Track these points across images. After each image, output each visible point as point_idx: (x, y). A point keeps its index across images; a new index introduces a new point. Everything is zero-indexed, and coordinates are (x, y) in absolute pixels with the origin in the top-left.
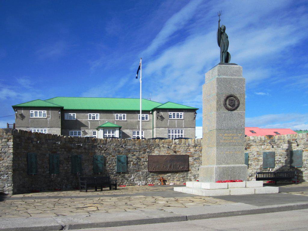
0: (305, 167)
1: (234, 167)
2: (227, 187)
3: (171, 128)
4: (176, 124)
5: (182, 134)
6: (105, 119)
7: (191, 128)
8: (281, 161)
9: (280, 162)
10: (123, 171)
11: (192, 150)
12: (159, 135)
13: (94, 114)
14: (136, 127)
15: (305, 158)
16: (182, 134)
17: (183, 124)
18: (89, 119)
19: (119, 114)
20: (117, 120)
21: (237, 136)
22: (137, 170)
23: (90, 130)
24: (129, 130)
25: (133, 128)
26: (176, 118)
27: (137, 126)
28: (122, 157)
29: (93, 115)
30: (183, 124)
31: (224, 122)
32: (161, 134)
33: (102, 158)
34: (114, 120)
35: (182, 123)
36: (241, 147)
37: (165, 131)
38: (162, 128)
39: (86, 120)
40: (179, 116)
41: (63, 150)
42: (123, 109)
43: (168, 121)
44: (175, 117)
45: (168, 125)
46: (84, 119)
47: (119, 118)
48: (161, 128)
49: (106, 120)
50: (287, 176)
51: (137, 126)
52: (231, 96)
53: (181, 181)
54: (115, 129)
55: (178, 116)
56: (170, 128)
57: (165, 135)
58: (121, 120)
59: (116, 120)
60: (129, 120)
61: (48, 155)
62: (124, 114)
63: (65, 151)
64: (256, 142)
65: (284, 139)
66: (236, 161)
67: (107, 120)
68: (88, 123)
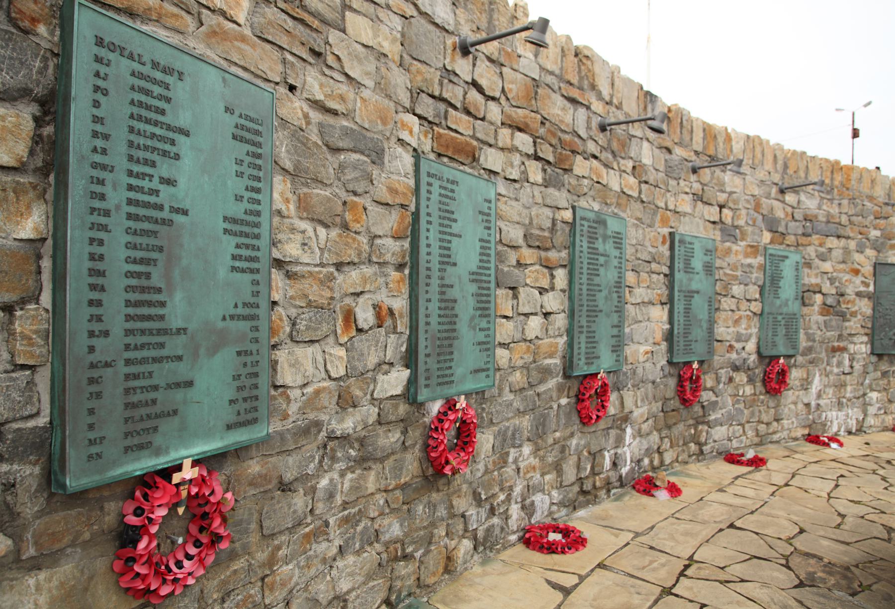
22: (836, 344)
41: (523, 141)
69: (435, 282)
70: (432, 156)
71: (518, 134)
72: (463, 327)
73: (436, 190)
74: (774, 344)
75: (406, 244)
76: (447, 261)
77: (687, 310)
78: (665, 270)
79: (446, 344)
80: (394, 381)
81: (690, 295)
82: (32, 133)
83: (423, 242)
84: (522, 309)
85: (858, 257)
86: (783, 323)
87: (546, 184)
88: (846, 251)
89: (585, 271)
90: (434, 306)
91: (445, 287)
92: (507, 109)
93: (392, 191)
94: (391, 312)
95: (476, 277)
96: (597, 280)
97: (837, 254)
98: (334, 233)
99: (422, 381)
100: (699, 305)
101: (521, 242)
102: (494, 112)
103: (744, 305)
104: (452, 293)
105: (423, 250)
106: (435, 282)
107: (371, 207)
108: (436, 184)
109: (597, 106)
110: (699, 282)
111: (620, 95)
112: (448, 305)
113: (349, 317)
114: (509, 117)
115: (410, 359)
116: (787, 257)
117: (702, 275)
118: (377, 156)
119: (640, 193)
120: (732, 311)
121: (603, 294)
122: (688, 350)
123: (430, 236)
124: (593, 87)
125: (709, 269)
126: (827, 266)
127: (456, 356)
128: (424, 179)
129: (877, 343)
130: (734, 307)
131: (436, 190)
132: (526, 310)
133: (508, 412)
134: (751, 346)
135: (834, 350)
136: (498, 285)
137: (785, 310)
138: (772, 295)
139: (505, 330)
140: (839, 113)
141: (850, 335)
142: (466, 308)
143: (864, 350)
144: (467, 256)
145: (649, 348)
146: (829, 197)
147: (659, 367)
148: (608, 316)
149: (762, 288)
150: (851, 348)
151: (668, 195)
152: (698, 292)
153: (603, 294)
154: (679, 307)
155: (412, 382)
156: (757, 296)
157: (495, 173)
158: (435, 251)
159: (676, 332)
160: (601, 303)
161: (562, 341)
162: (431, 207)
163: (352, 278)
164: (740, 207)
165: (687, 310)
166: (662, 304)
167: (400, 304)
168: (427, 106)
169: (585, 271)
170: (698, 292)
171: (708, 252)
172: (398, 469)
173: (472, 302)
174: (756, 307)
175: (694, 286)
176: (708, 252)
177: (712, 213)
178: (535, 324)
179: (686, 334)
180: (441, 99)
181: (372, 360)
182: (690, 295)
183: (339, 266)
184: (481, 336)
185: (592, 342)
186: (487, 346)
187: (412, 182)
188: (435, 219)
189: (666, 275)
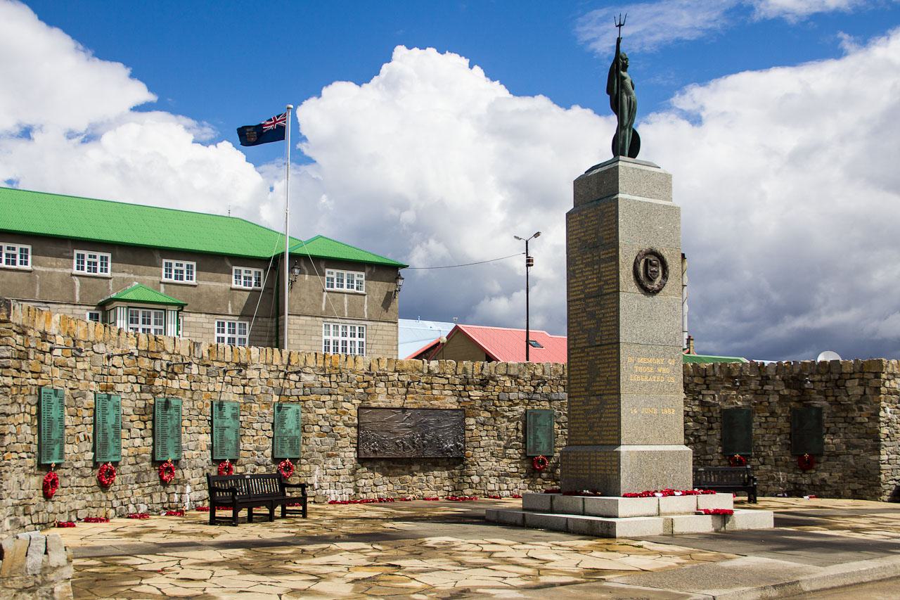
0: (757, 456)
1: (662, 453)
2: (655, 511)
3: (332, 320)
4: (346, 306)
5: (221, 335)
6: (128, 273)
7: (386, 324)
8: (702, 438)
9: (697, 441)
10: (292, 457)
11: (476, 394)
12: (297, 337)
13: (11, 245)
14: (227, 308)
15: (758, 432)
16: (221, 335)
17: (366, 307)
18: (75, 271)
19: (174, 262)
20: (168, 280)
21: (667, 365)
22: (330, 453)
23: (78, 307)
24: (203, 315)
25: (218, 310)
26: (345, 289)
27: (230, 305)
28: (290, 410)
29: (9, 248)
30: (366, 307)
31: (637, 325)
32: (302, 337)
33: (235, 411)
34: (157, 279)
35: (362, 306)
36: (676, 396)
37: (314, 328)
38: (305, 318)
39: (68, 271)
40: (353, 282)
41: (132, 379)
42: (227, 252)
43: (322, 295)
44: (342, 286)
45: (323, 309)
46: (60, 267)
47: (173, 273)
48: (302, 318)
49: (132, 276)
50: (716, 480)
51: (230, 305)
52: (653, 253)
53: (447, 488)
54: (165, 310)
55: (350, 281)
56: (329, 320)
57: (313, 338)
58: (179, 282)
59: (164, 279)
60: (205, 283)
61: (90, 398)
62: (190, 263)
63: (137, 383)
64: (701, 401)
65: (706, 376)
66: (666, 436)
67: (137, 277)
68: (74, 284)
69: (101, 428)
70: (99, 392)
71: (130, 376)
72: (110, 442)
73: (101, 402)
74: (282, 452)
75: (92, 418)
76: (104, 422)
77: (222, 436)
78: (210, 418)
79: (105, 446)
80: (90, 455)
81: (223, 429)
82: (761, 570)
83: (97, 417)
84: (132, 436)
85: (345, 405)
86: (288, 441)
87: (142, 391)
88: (336, 402)
89: (160, 421)
90: (101, 435)
91: (104, 430)
92: (126, 369)
93: (89, 405)
94: (88, 437)
95: (114, 426)
96: (166, 425)
97: (330, 404)
98: (75, 418)
99: (97, 456)
100: (230, 435)
101: (132, 413)
102: (120, 372)
103: (261, 433)
104: (107, 431)
105: (97, 420)
106: (101, 428)
107: (83, 410)
108: (101, 400)
109: (166, 357)
110: (229, 422)
111: (178, 349)
112: (105, 435)
113: (78, 438)
114: (126, 371)
115: (94, 450)
116: (290, 408)
117: (231, 419)
118: (84, 396)
119: (191, 386)
120: (253, 436)
121: (169, 430)
122: (223, 453)
123: (99, 415)
124: (164, 350)
125: (235, 416)
126: (323, 411)
127: (108, 450)
128: (97, 400)
129: (362, 452)
130: (255, 434)
131: (101, 402)
132: (134, 436)
133: (126, 469)
134: (268, 452)
135: (329, 456)
136: (122, 428)
137: (289, 435)
138: (279, 427)
139: (124, 443)
140: (516, 240)
141: (342, 447)
142: (111, 436)
143: (353, 456)
144: (111, 420)
145: (198, 452)
146: (322, 373)
147: (205, 461)
148: (172, 438)
149: (273, 425)
150: (342, 454)
151: (209, 384)
152: (228, 427)
153: (169, 430)
154: (216, 434)
155: (95, 456)
156: (270, 428)
157: (121, 392)
158: (101, 419)
159: (214, 446)
160: (168, 432)
161: (150, 449)
162: (99, 408)
163: (78, 429)
164: (257, 385)
165: (222, 436)
166: (207, 433)
167: (91, 435)
168: (98, 378)
169: (160, 421)
170: (228, 427)
171: (234, 408)
172: (91, 481)
173: (113, 434)
174: (271, 434)
175: (226, 425)
176: (234, 408)
177: (240, 389)
178: (138, 442)
179: (221, 446)
180: (102, 374)
181: (84, 450)
182: (223, 429)
183: (76, 425)
184: (116, 444)
185: (164, 448)
186: (119, 448)
187: (94, 401)
188: (101, 411)
189: (209, 421)
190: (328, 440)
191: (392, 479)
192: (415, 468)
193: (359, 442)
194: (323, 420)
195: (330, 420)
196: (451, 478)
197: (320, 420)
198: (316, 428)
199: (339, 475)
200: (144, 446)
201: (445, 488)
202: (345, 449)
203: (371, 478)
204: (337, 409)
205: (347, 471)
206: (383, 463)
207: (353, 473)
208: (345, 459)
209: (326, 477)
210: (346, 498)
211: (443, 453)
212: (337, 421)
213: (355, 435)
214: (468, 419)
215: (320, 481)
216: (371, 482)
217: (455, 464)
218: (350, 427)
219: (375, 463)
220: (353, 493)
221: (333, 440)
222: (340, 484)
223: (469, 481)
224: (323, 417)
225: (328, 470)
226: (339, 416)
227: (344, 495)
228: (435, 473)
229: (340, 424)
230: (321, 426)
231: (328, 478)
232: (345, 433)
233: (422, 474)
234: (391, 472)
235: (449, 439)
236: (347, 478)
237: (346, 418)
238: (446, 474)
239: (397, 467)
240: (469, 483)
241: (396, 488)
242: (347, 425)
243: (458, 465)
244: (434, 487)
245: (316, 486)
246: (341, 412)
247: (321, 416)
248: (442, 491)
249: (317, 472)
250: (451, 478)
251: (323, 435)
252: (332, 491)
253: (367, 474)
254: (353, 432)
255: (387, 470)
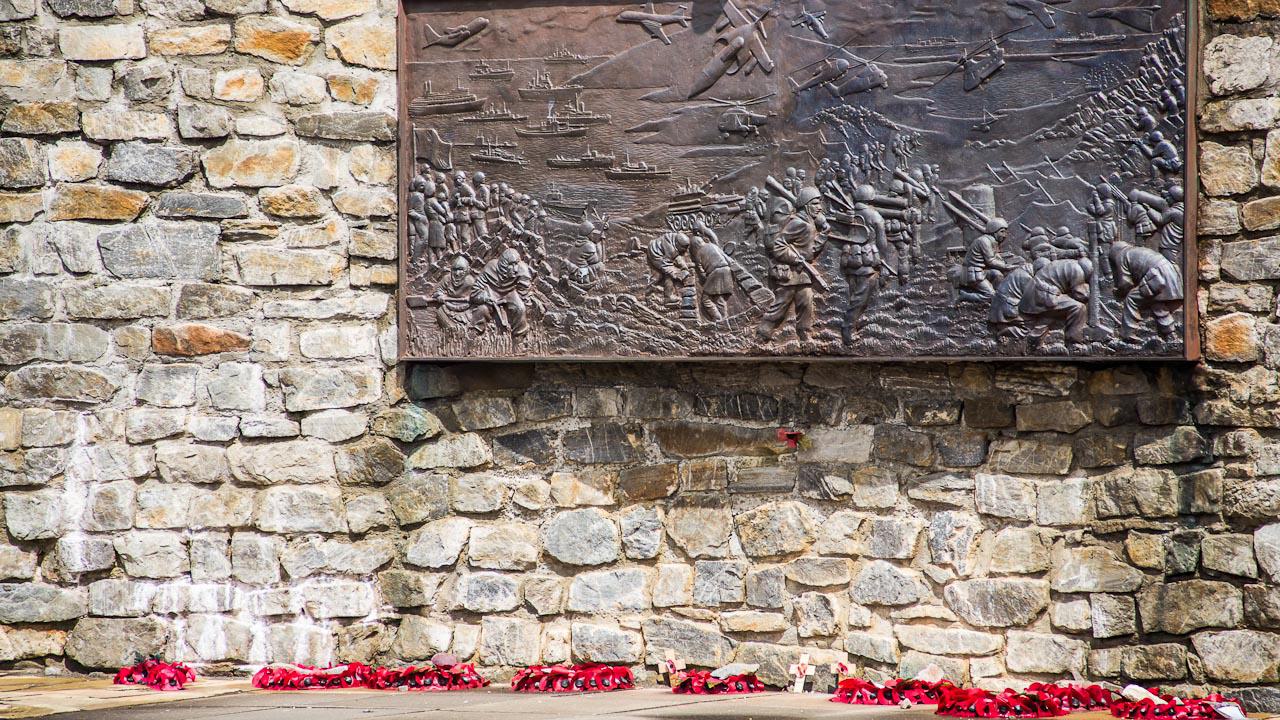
22: (179, 327)
53: (1074, 614)
135: (176, 352)
150: (278, 340)
190: (156, 236)
191: (689, 523)
192: (843, 440)
193: (421, 254)
194: (119, 103)
195: (176, 99)
196: (1108, 532)
197: (97, 104)
198: (67, 160)
199: (258, 485)
200: (191, 428)
201: (1062, 614)
202: (300, 304)
203: (527, 513)
204: (230, 18)
205: (320, 456)
206: (611, 403)
207: (382, 466)
208: (297, 370)
209: (153, 492)
210: (313, 645)
211: (995, 327)
212: (240, 108)
213: (381, 199)
214: (1225, 40)
215: (105, 521)
216: (522, 539)
217: (1133, 424)
218: (344, 142)
219: (551, 403)
220: (368, 602)
221: (200, 239)
222: (264, 542)
223: (1242, 564)
224: (119, 82)
225: (166, 449)
226: (251, 73)
227: (303, 624)
228: (990, 485)
229: (266, 120)
230: (107, 147)
231: (177, 502)
232: (306, 184)
233: (890, 494)
234: (687, 466)
235: (1055, 218)
236: (320, 507)
237: (303, 81)
238: (1073, 498)
239: (717, 437)
240: (1240, 580)
241: (710, 593)
242: (314, 134)
243: (1163, 428)
244: (983, 601)
245: (76, 551)
246: (266, 38)
247: (103, 75)
248: (1040, 633)
249: (78, 459)
250: (1108, 532)
251: (111, 202)
252: (203, 593)
253: (492, 479)
254: (365, 178)
255: (655, 454)
